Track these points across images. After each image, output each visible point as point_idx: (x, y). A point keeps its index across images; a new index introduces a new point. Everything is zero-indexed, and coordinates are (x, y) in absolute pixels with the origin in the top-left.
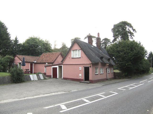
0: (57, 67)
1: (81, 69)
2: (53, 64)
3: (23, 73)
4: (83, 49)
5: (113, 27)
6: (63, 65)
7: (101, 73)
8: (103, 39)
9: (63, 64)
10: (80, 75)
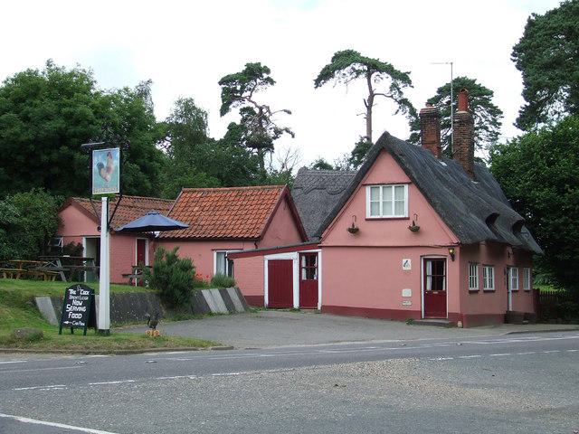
0: (294, 256)
1: (408, 268)
2: (264, 245)
3: (202, 285)
4: (420, 183)
5: (517, 34)
6: (325, 249)
7: (488, 288)
8: (442, 84)
9: (323, 244)
10: (407, 293)
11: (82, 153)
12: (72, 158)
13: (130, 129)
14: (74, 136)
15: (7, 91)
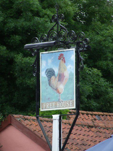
11: (26, 55)
12: (11, 62)
13: (88, 21)
14: (15, 32)
15: (46, 150)
